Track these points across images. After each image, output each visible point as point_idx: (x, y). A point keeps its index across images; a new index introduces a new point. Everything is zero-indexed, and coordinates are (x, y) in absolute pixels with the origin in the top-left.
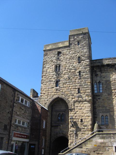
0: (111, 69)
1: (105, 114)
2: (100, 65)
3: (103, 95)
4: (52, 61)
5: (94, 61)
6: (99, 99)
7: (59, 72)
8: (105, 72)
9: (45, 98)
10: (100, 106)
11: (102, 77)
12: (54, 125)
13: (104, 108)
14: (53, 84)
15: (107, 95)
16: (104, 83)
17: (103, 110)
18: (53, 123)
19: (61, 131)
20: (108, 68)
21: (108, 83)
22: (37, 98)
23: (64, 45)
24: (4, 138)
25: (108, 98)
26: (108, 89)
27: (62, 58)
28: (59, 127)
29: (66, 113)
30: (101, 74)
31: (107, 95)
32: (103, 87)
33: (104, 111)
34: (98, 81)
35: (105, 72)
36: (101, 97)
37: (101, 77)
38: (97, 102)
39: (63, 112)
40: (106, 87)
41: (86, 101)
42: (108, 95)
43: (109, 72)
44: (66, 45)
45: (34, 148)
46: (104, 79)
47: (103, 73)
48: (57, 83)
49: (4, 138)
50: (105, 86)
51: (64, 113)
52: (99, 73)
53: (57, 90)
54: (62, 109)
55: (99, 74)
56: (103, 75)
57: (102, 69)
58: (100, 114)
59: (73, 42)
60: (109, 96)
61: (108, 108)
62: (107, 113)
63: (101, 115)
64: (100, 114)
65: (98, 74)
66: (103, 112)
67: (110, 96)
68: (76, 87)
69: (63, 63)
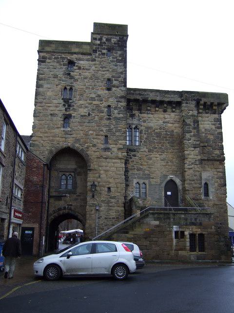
0: (157, 109)
3: (141, 150)
4: (56, 76)
5: (132, 92)
6: (135, 156)
7: (70, 101)
11: (141, 120)
12: (54, 194)
14: (59, 120)
18: (51, 190)
20: (153, 106)
23: (81, 51)
24: (5, 219)
31: (147, 150)
32: (141, 138)
34: (134, 126)
36: (72, 112)
38: (130, 160)
41: (117, 158)
42: (149, 152)
43: (153, 113)
44: (85, 51)
45: (32, 235)
46: (145, 124)
47: (144, 113)
48: (67, 118)
49: (5, 219)
52: (136, 113)
53: (66, 133)
54: (68, 167)
55: (137, 115)
56: (143, 117)
57: (143, 107)
60: (150, 153)
61: (146, 172)
63: (135, 181)
65: (134, 114)
66: (139, 178)
67: (152, 153)
68: (101, 133)
69: (77, 86)
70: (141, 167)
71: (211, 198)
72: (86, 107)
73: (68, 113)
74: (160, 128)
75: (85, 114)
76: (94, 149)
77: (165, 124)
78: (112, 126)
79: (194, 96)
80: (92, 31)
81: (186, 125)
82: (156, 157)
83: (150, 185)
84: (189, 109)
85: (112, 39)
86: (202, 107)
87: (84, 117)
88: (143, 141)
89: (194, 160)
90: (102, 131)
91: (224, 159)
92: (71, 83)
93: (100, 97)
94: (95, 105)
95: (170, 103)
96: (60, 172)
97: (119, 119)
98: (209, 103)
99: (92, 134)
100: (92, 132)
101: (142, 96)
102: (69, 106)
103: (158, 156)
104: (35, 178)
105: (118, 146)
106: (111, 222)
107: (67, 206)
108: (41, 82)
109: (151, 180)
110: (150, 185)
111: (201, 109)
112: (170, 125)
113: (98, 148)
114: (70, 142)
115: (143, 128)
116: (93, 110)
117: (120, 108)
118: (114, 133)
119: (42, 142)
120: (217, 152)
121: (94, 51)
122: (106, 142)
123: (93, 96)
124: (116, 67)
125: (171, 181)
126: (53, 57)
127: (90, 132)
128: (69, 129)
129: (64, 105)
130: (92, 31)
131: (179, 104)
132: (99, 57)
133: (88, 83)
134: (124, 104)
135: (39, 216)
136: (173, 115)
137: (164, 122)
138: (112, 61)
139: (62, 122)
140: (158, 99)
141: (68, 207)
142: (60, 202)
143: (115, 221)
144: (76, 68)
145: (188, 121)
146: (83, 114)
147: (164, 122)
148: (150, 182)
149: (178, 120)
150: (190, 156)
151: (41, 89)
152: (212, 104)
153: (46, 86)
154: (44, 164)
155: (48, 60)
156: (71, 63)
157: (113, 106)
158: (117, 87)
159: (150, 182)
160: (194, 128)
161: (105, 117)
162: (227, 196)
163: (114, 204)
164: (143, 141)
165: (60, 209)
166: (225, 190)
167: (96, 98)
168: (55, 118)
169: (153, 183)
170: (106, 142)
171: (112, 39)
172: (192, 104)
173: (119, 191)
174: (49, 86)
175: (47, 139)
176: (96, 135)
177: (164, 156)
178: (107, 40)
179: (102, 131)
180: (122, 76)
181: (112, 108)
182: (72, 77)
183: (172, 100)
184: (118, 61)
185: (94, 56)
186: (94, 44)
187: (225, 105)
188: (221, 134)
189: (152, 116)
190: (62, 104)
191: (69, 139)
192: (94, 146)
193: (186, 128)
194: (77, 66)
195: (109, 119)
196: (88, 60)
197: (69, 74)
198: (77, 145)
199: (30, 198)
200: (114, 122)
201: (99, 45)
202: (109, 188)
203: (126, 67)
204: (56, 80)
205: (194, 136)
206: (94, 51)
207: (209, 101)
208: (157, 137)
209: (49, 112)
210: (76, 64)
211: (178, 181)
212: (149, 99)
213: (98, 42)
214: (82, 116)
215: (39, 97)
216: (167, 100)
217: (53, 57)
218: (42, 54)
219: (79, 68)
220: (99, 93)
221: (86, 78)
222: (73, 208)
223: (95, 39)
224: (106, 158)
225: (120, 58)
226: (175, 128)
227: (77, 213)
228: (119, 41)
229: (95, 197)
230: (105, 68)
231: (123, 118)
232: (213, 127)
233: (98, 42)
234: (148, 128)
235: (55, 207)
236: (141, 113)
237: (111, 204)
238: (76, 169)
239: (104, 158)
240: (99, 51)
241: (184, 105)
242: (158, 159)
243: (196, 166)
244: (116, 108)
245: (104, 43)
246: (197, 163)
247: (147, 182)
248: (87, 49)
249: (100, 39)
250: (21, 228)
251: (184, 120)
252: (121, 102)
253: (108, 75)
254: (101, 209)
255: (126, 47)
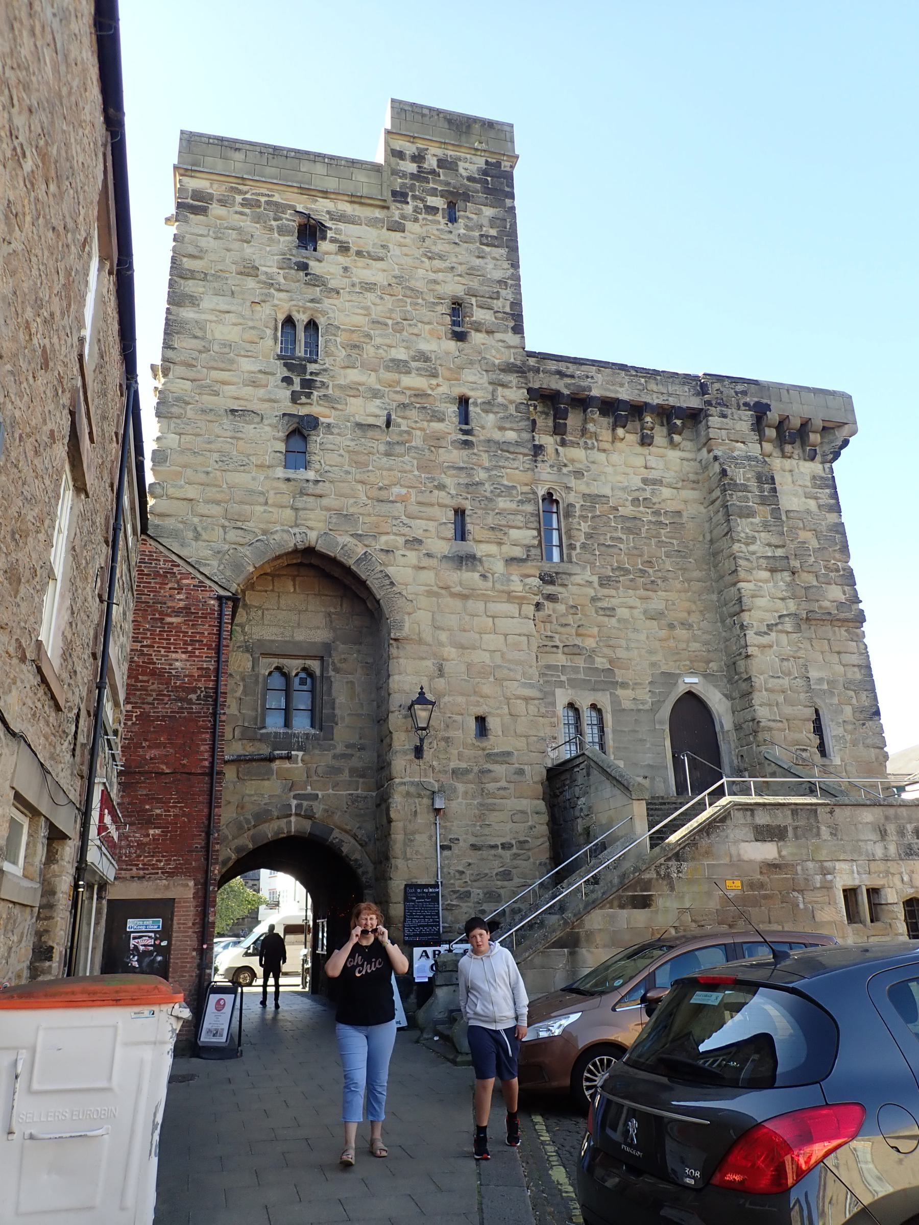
1: (587, 693)
2: (566, 392)
3: (577, 579)
4: (250, 270)
7: (311, 367)
8: (582, 443)
9: (266, 503)
10: (557, 647)
11: (565, 470)
13: (580, 662)
14: (269, 440)
15: (596, 585)
16: (578, 506)
17: (576, 669)
19: (295, 797)
21: (598, 513)
22: (398, 235)
23: (349, 187)
25: (600, 604)
26: (603, 548)
27: (327, 262)
28: (276, 765)
29: (337, 670)
30: (560, 449)
31: (595, 579)
33: (582, 676)
35: (582, 443)
36: (560, 589)
37: (560, 470)
39: (309, 662)
40: (589, 536)
42: (601, 585)
46: (580, 486)
48: (300, 432)
50: (584, 527)
51: (315, 665)
56: (573, 461)
57: (573, 420)
58: (559, 692)
59: (412, 187)
60: (606, 591)
61: (601, 662)
62: (600, 693)
64: (559, 692)
67: (613, 592)
69: (341, 313)
70: (578, 641)
71: (837, 761)
72: (376, 394)
73: (303, 411)
74: (635, 501)
75: (371, 420)
76: (412, 557)
77: (648, 488)
78: (482, 475)
79: (744, 393)
80: (389, 127)
81: (734, 486)
82: (627, 601)
83: (618, 711)
84: (731, 432)
85: (457, 171)
86: (771, 433)
87: (370, 434)
88: (578, 544)
89: (776, 615)
90: (441, 487)
91: (860, 618)
92: (312, 301)
93: (427, 359)
94: (409, 389)
95: (666, 414)
96: (264, 655)
97: (503, 447)
98: (796, 423)
99: (403, 500)
100: (404, 491)
101: (568, 381)
102: (308, 384)
103: (637, 603)
104: (180, 662)
105: (505, 548)
106: (496, 863)
107: (294, 803)
108: (190, 287)
109: (619, 692)
110: (618, 711)
111: (769, 441)
112: (666, 492)
113: (429, 555)
114: (314, 530)
115: (572, 498)
116: (404, 406)
117: (505, 407)
118: (490, 500)
119: (196, 520)
120: (836, 593)
121: (394, 193)
122: (461, 534)
123: (401, 354)
124: (478, 262)
125: (691, 696)
126: (239, 198)
127: (396, 490)
128: (311, 475)
129: (287, 380)
130: (389, 127)
131: (694, 417)
132: (416, 220)
133: (380, 307)
134: (516, 394)
135: (198, 843)
136: (674, 455)
137: (645, 481)
138: (466, 240)
139: (282, 447)
140: (624, 393)
141: (299, 806)
142: (266, 783)
143: (516, 856)
144: (333, 247)
145: (740, 475)
146: (360, 419)
147: (645, 481)
148: (615, 701)
149: (692, 477)
150: (760, 602)
151: (187, 313)
152: (805, 425)
153: (209, 302)
154: (220, 598)
155: (216, 209)
156: (310, 232)
157: (477, 396)
158: (490, 332)
159: (615, 701)
160: (763, 501)
161: (450, 438)
162: (886, 757)
163: (503, 784)
164: (578, 550)
165: (262, 817)
166: (880, 731)
167: (414, 364)
168: (249, 430)
169: (627, 704)
170: (461, 534)
171: (457, 171)
172: (743, 422)
173: (520, 729)
174: (222, 303)
175: (216, 510)
176: (420, 503)
177: (657, 602)
178: (442, 163)
179: (441, 487)
180: (503, 293)
181: (475, 404)
182: (316, 281)
183: (672, 401)
184: (485, 240)
185: (397, 212)
186: (395, 172)
187: (846, 430)
188: (839, 529)
189: (602, 457)
190: (279, 376)
191: (311, 515)
192: (414, 543)
193: (735, 500)
194: (333, 241)
195: (467, 444)
196: (373, 223)
197: (303, 267)
198: (344, 539)
199: (153, 753)
200: (485, 456)
201: (413, 176)
202: (481, 721)
203: (515, 265)
204: (251, 283)
205: (766, 526)
206: (394, 193)
207: (797, 412)
208: (629, 531)
209: (224, 402)
210: (329, 234)
211: (718, 702)
212: (595, 392)
213: (412, 167)
214: (359, 425)
215: (182, 343)
216: (655, 400)
217: (239, 198)
218: (193, 184)
219: (344, 249)
220: (424, 346)
221: (369, 287)
222: (319, 809)
223: (400, 155)
224: (465, 597)
225: (493, 232)
226: (683, 500)
227: (336, 833)
228: (485, 173)
229: (428, 754)
230: (441, 257)
231: (517, 444)
232: (812, 504)
233: (412, 167)
234: (593, 499)
235: (241, 806)
236: (563, 443)
237: (491, 787)
238: (328, 647)
239: (454, 595)
240: (414, 197)
241: (714, 421)
242: (636, 612)
243: (784, 638)
244: (489, 406)
245: (433, 172)
246: (788, 627)
247: (604, 700)
248: (363, 183)
249: (418, 158)
250: (104, 902)
251: (724, 473)
252: (503, 385)
253: (454, 287)
254: (454, 804)
255: (512, 196)
